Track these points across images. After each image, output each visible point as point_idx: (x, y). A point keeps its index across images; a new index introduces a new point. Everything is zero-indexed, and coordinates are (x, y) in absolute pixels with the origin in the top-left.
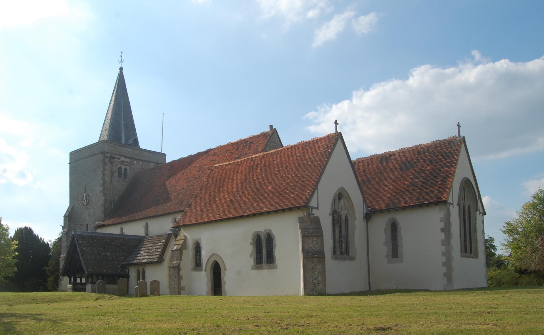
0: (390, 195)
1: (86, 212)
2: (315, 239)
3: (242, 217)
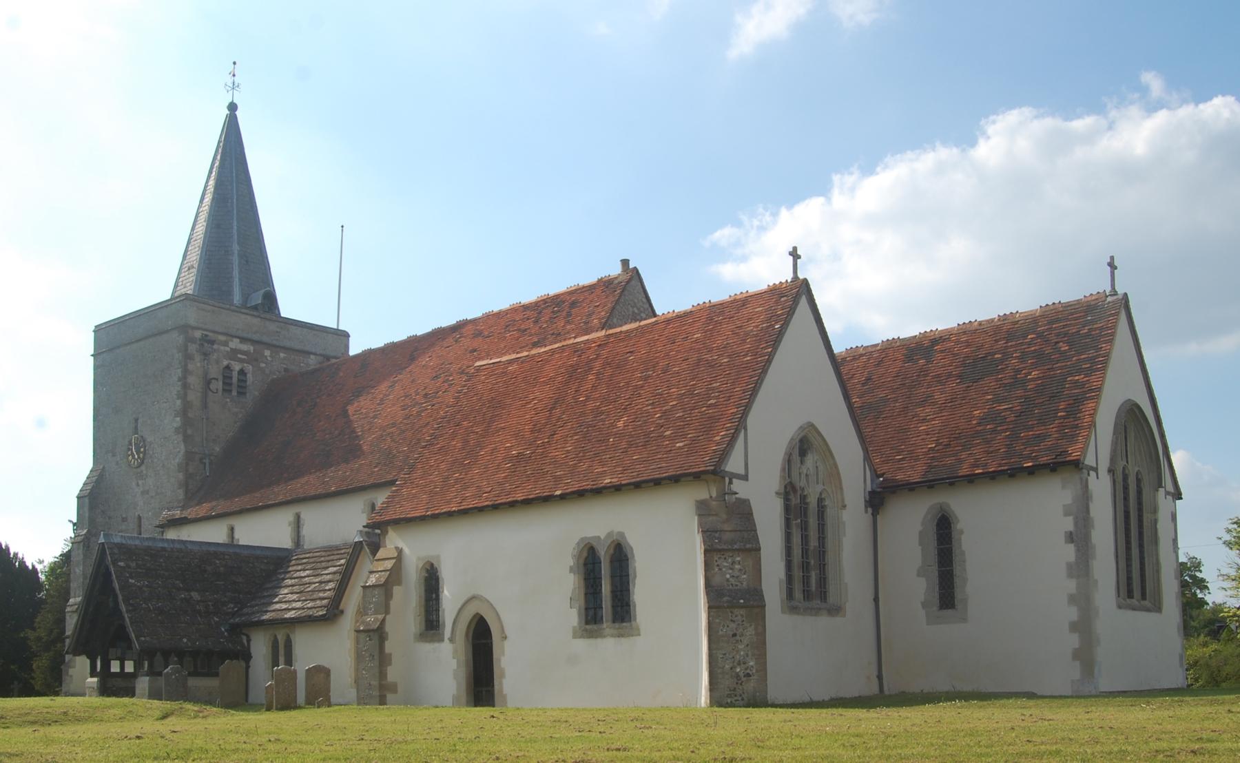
0: (934, 445)
1: (138, 485)
2: (738, 559)
3: (547, 500)
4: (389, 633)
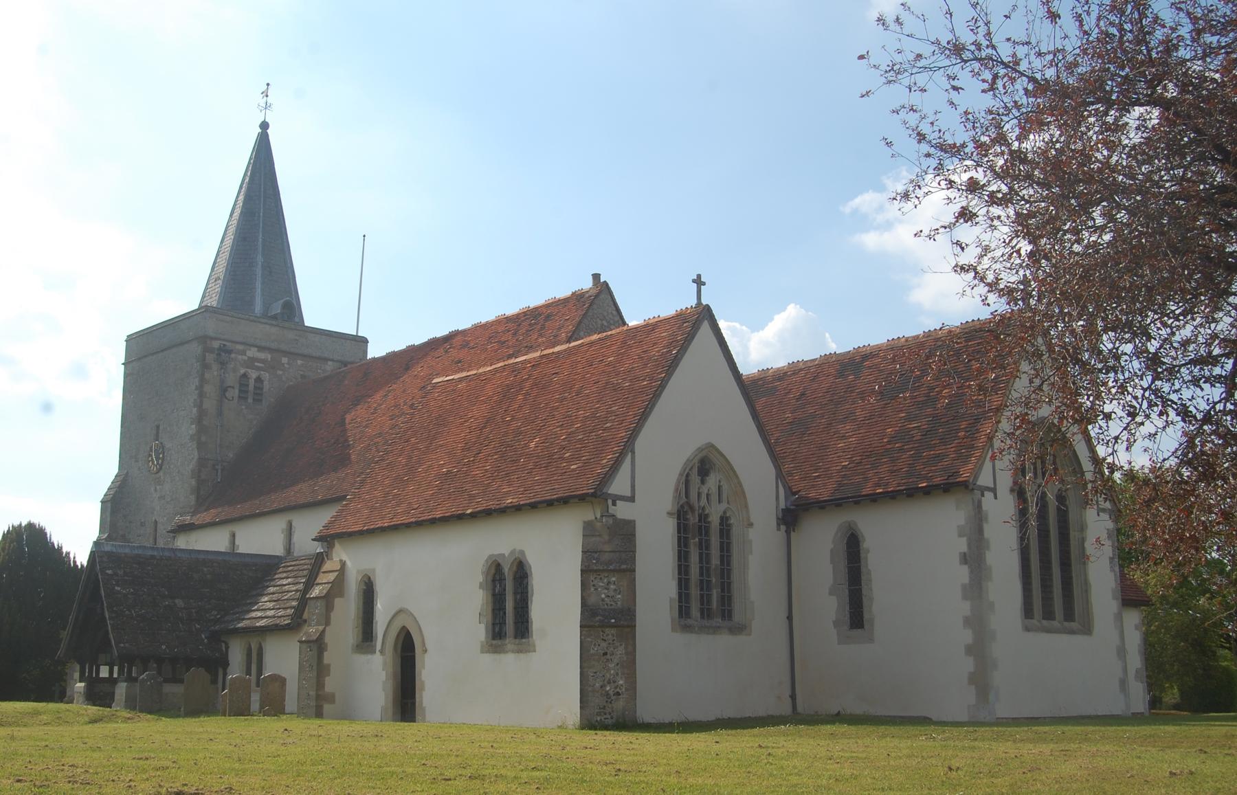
0: (847, 463)
1: (156, 490)
2: (614, 579)
3: (460, 518)
4: (329, 644)
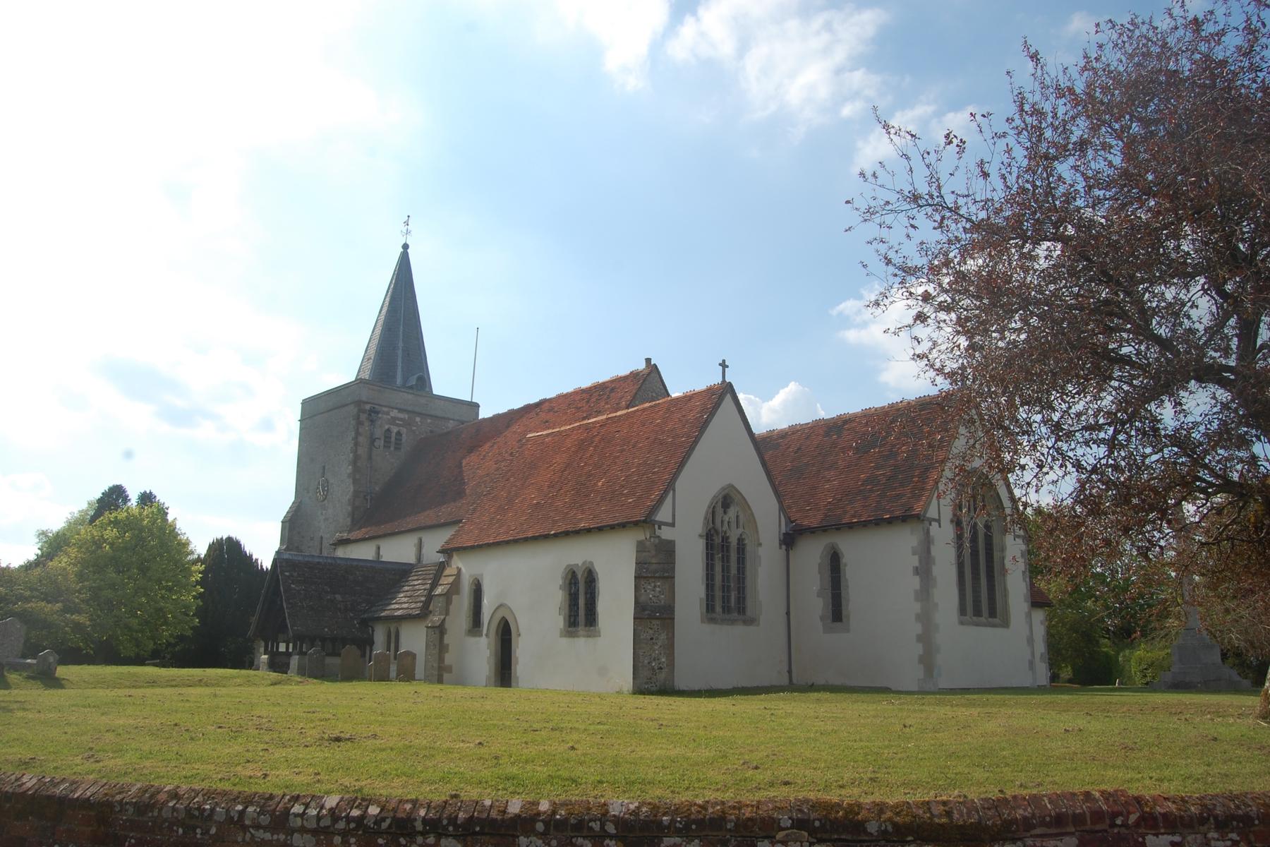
1: (322, 514)
3: (546, 537)
